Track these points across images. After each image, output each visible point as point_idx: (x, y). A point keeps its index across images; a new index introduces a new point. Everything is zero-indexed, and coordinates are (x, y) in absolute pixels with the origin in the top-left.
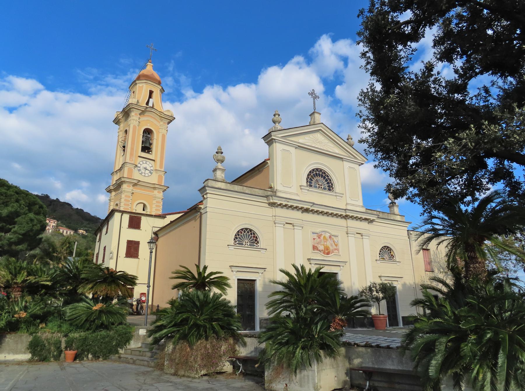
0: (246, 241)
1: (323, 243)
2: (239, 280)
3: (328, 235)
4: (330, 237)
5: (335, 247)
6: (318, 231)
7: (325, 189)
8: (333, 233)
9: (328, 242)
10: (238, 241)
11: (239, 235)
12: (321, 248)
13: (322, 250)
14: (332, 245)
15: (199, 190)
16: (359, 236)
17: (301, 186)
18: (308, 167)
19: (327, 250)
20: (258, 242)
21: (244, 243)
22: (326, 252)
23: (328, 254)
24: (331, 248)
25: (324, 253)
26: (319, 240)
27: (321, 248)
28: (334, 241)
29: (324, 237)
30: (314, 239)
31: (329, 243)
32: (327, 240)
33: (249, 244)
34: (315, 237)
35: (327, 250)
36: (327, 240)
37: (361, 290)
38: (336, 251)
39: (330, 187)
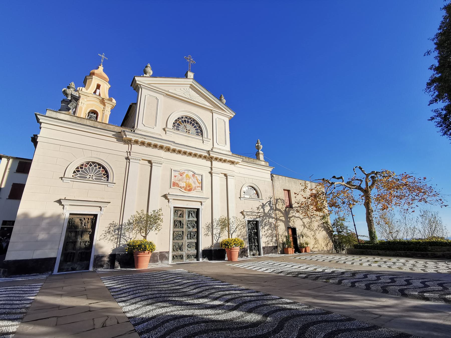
1: (185, 180)
9: (191, 180)
10: (80, 174)
11: (82, 168)
12: (183, 184)
13: (183, 187)
14: (195, 183)
19: (189, 187)
22: (188, 188)
23: (190, 190)
24: (194, 185)
25: (185, 190)
27: (183, 184)
28: (197, 180)
29: (187, 175)
32: (190, 178)
36: (190, 178)
39: (200, 131)
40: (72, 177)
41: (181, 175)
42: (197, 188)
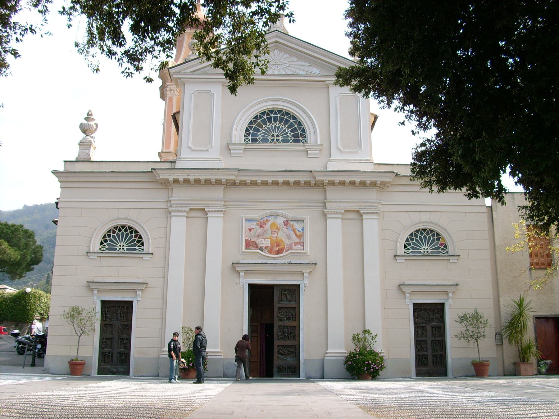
0: (122, 245)
1: (269, 234)
2: (249, 285)
3: (280, 221)
4: (286, 223)
5: (297, 240)
6: (258, 214)
7: (285, 141)
8: (291, 215)
9: (280, 233)
13: (266, 247)
14: (289, 237)
15: (65, 161)
16: (353, 216)
17: (87, 252)
18: (247, 111)
19: (278, 245)
20: (142, 244)
21: (118, 248)
24: (287, 242)
25: (270, 252)
26: (260, 230)
27: (265, 242)
28: (294, 230)
29: (273, 224)
30: (250, 230)
31: (282, 235)
33: (125, 248)
34: (253, 227)
35: (278, 245)
36: (278, 229)
37: (510, 319)
38: (299, 246)
39: (298, 133)
40: (405, 254)
41: (261, 227)
42: (294, 247)
